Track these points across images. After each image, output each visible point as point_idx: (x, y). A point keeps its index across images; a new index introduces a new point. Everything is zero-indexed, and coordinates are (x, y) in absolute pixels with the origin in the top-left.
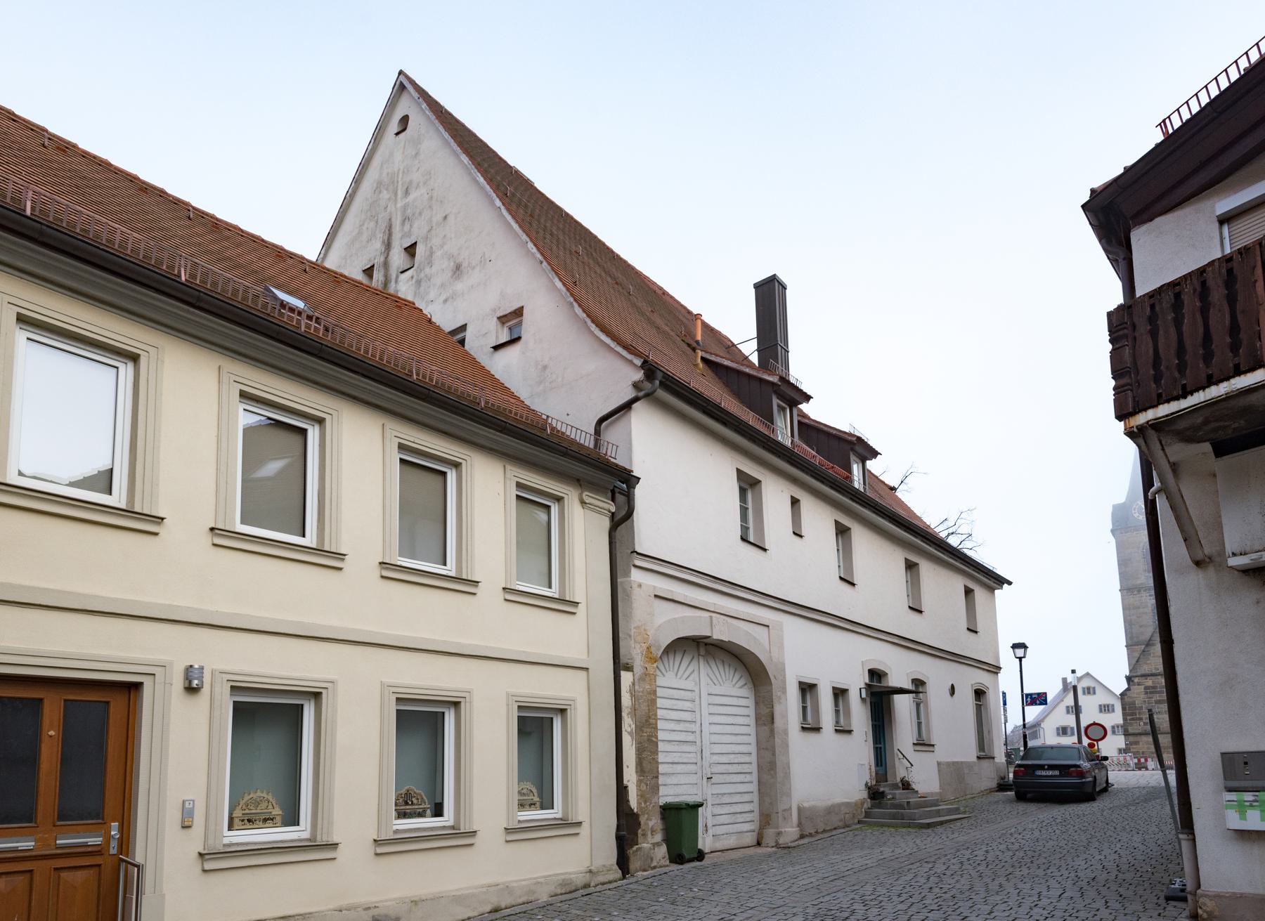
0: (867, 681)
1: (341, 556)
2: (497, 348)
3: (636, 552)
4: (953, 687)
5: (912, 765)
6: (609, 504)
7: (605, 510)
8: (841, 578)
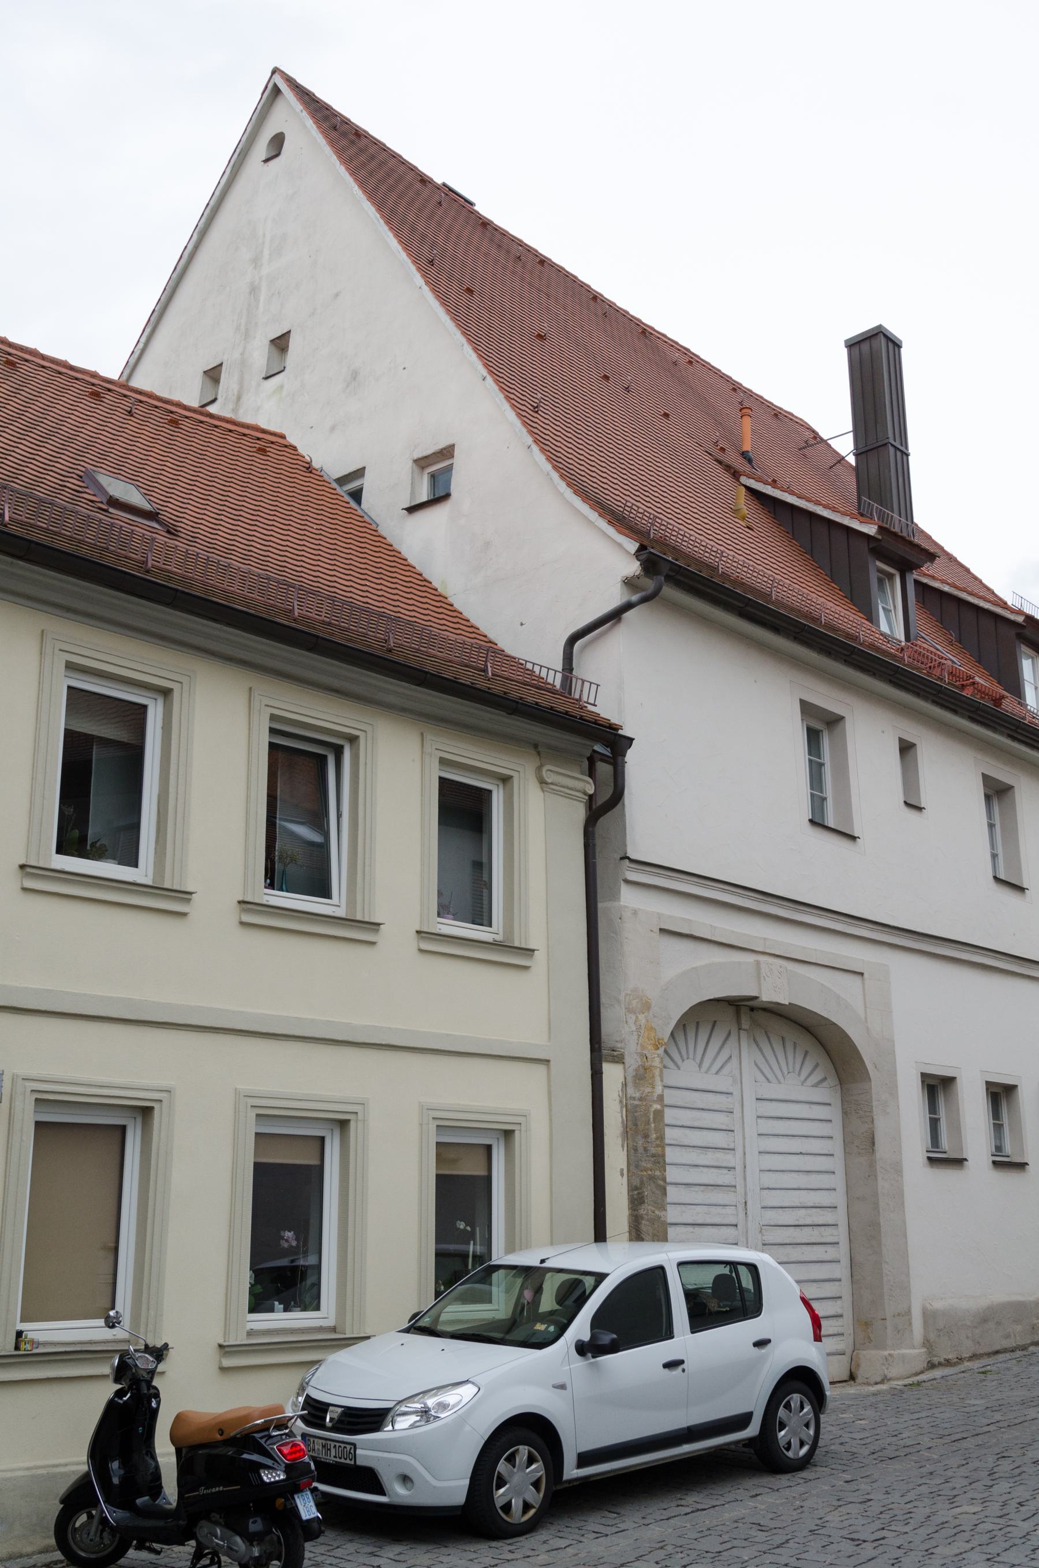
1: (185, 896)
2: (412, 510)
3: (628, 858)
6: (584, 781)
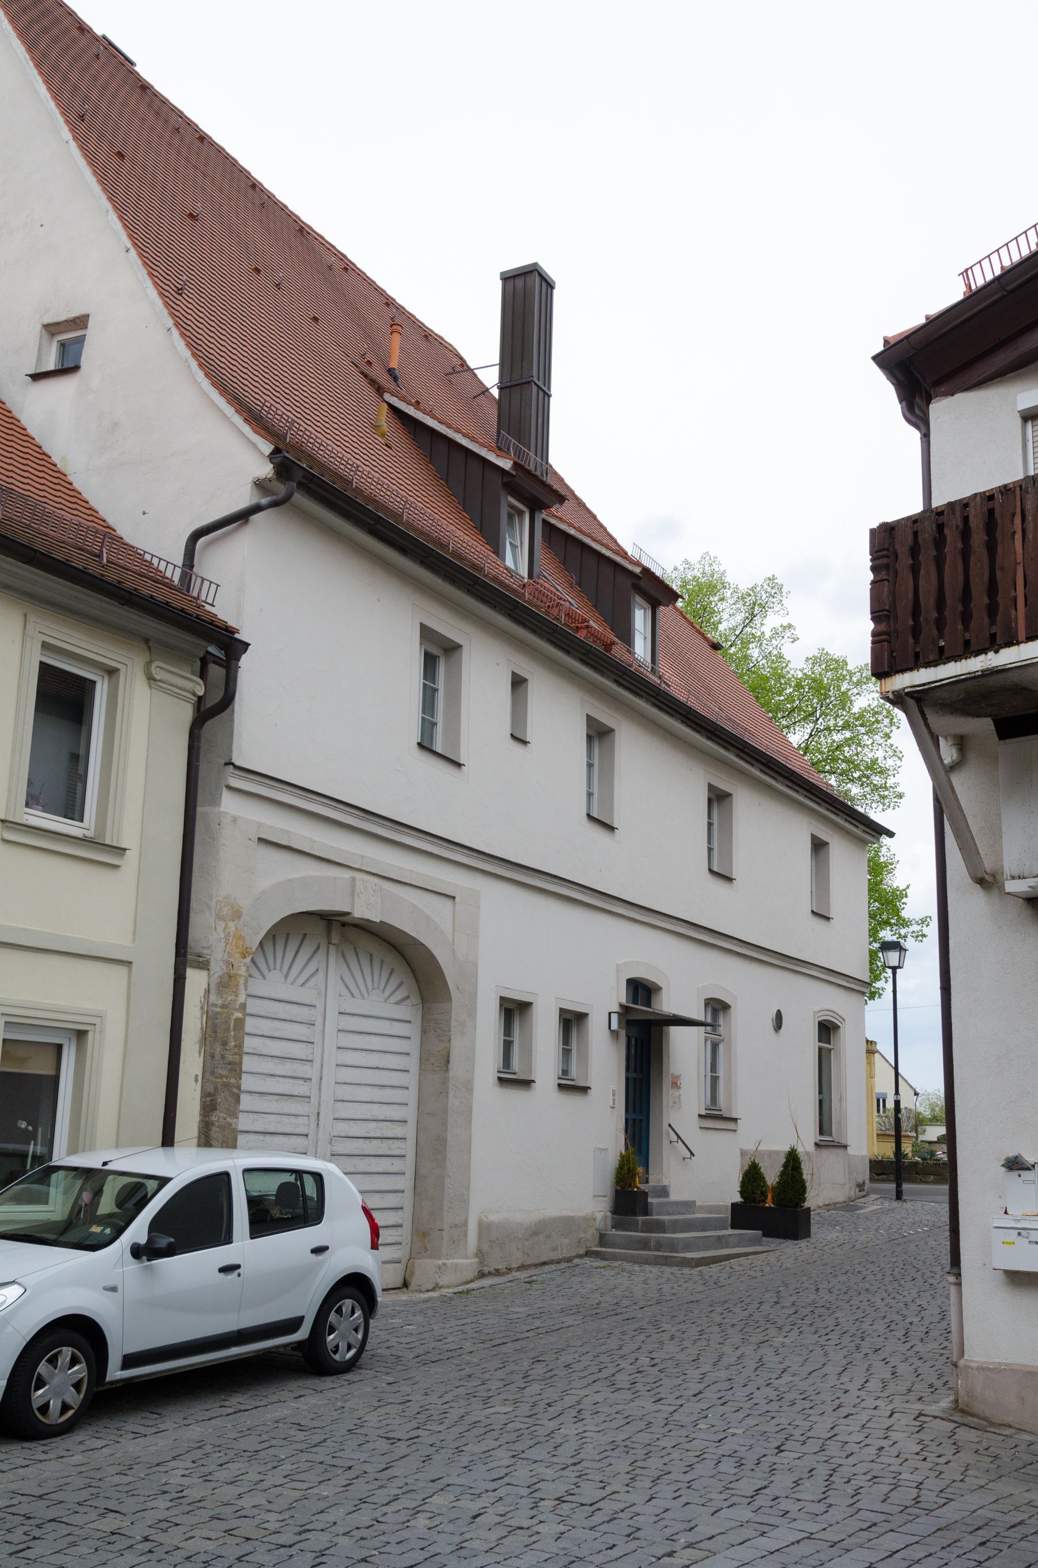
0: (624, 1001)
3: (233, 764)
4: (779, 1016)
5: (692, 1154)
7: (187, 691)
8: (590, 817)
